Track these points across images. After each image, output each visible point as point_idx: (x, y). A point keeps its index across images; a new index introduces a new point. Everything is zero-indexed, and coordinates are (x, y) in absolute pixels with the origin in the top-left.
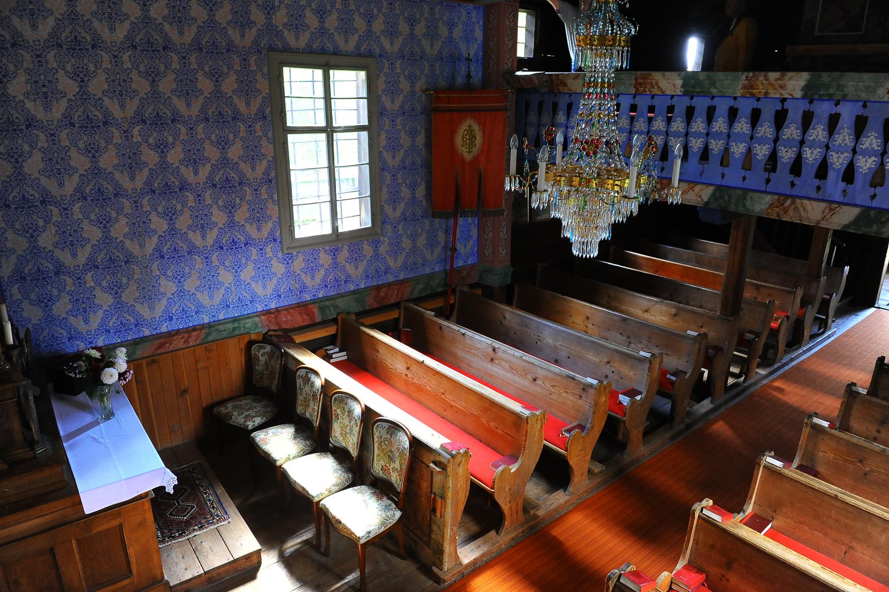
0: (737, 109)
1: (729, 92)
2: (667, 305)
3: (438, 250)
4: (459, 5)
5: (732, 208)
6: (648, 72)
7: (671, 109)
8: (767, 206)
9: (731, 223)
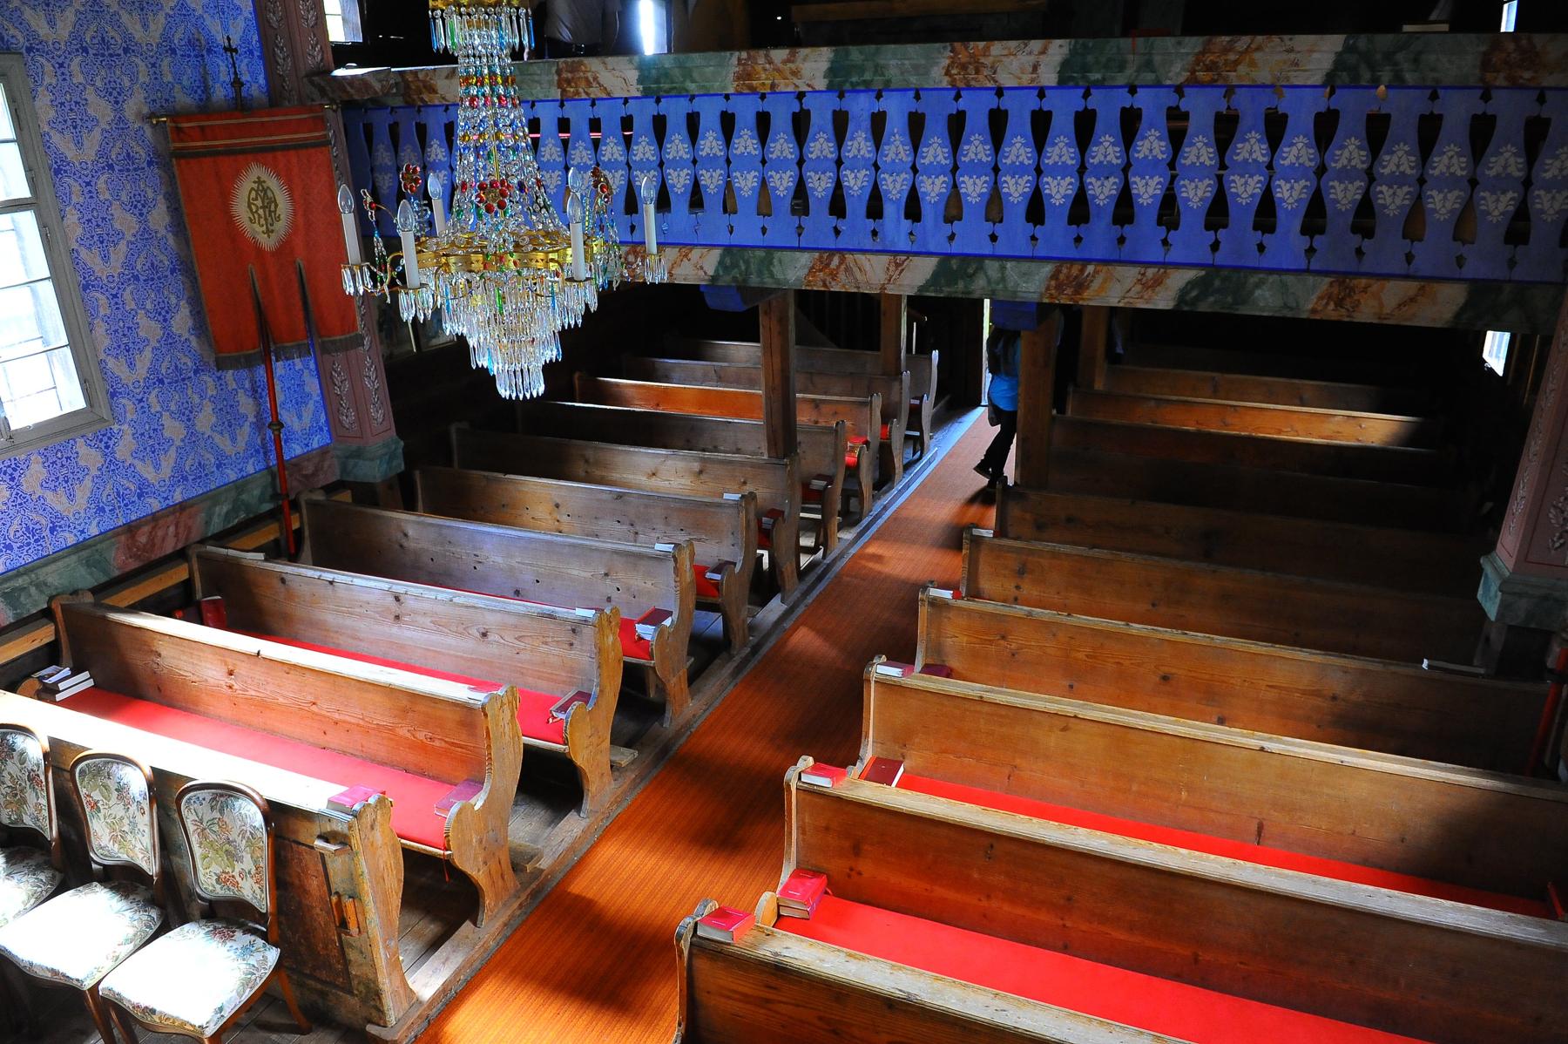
0: (733, 115)
1: (716, 87)
5: (754, 281)
7: (627, 123)
8: (806, 271)
9: (757, 307)
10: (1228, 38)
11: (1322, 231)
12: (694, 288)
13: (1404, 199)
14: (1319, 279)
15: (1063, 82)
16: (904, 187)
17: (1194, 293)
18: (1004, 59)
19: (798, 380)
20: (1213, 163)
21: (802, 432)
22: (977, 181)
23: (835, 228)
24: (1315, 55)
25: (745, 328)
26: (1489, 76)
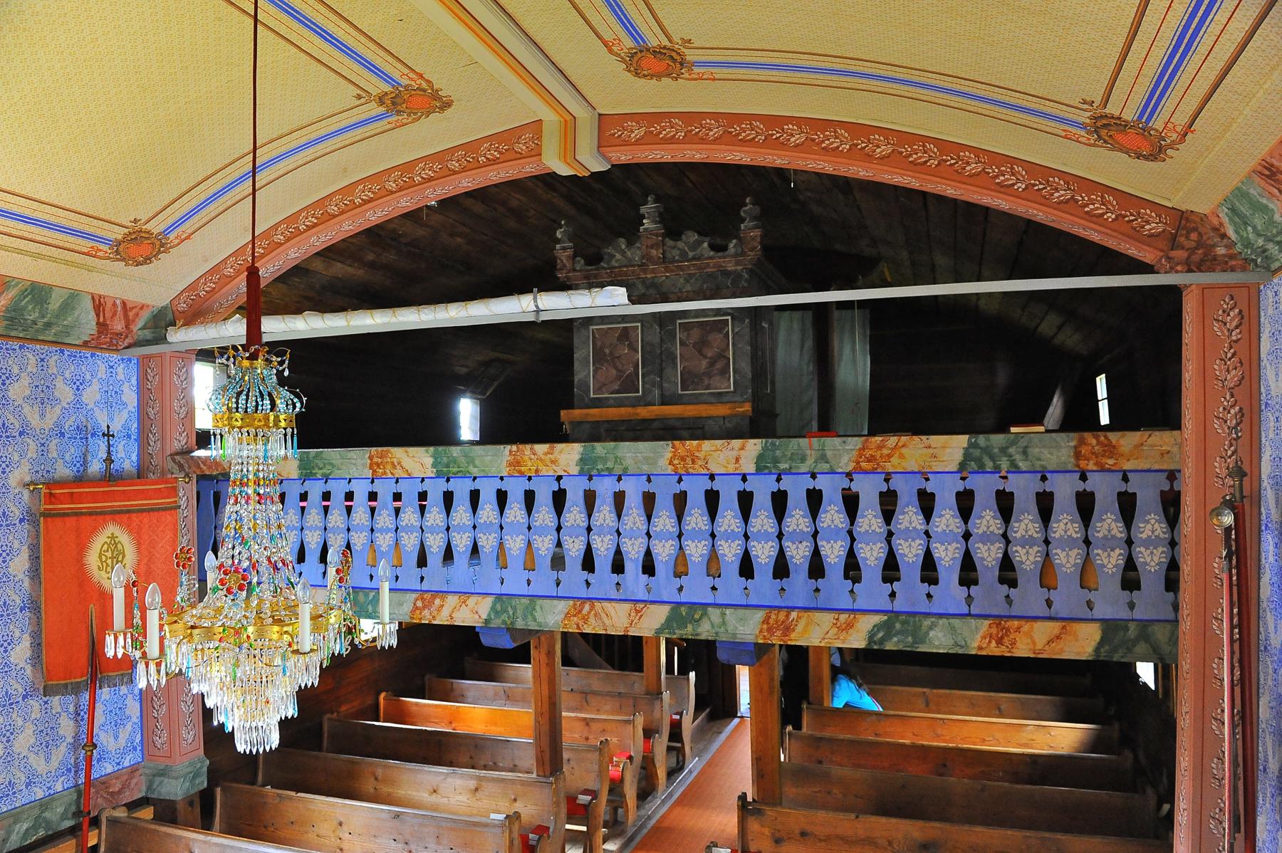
0: (506, 491)
1: (493, 471)
2: (462, 776)
3: (61, 753)
4: (93, 355)
5: (520, 624)
6: (385, 449)
7: (423, 496)
8: (563, 616)
9: (529, 642)
10: (881, 439)
11: (976, 583)
12: (470, 630)
13: (1036, 557)
14: (980, 621)
15: (760, 470)
16: (641, 549)
17: (880, 635)
18: (716, 454)
19: (565, 699)
20: (882, 530)
21: (568, 749)
22: (699, 544)
23: (587, 581)
24: (948, 450)
25: (521, 654)
26: (1083, 464)
